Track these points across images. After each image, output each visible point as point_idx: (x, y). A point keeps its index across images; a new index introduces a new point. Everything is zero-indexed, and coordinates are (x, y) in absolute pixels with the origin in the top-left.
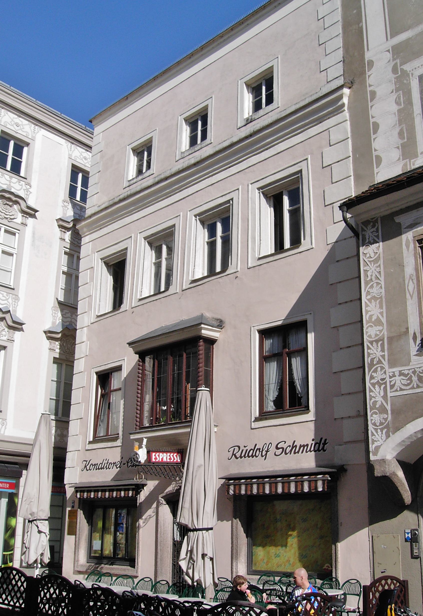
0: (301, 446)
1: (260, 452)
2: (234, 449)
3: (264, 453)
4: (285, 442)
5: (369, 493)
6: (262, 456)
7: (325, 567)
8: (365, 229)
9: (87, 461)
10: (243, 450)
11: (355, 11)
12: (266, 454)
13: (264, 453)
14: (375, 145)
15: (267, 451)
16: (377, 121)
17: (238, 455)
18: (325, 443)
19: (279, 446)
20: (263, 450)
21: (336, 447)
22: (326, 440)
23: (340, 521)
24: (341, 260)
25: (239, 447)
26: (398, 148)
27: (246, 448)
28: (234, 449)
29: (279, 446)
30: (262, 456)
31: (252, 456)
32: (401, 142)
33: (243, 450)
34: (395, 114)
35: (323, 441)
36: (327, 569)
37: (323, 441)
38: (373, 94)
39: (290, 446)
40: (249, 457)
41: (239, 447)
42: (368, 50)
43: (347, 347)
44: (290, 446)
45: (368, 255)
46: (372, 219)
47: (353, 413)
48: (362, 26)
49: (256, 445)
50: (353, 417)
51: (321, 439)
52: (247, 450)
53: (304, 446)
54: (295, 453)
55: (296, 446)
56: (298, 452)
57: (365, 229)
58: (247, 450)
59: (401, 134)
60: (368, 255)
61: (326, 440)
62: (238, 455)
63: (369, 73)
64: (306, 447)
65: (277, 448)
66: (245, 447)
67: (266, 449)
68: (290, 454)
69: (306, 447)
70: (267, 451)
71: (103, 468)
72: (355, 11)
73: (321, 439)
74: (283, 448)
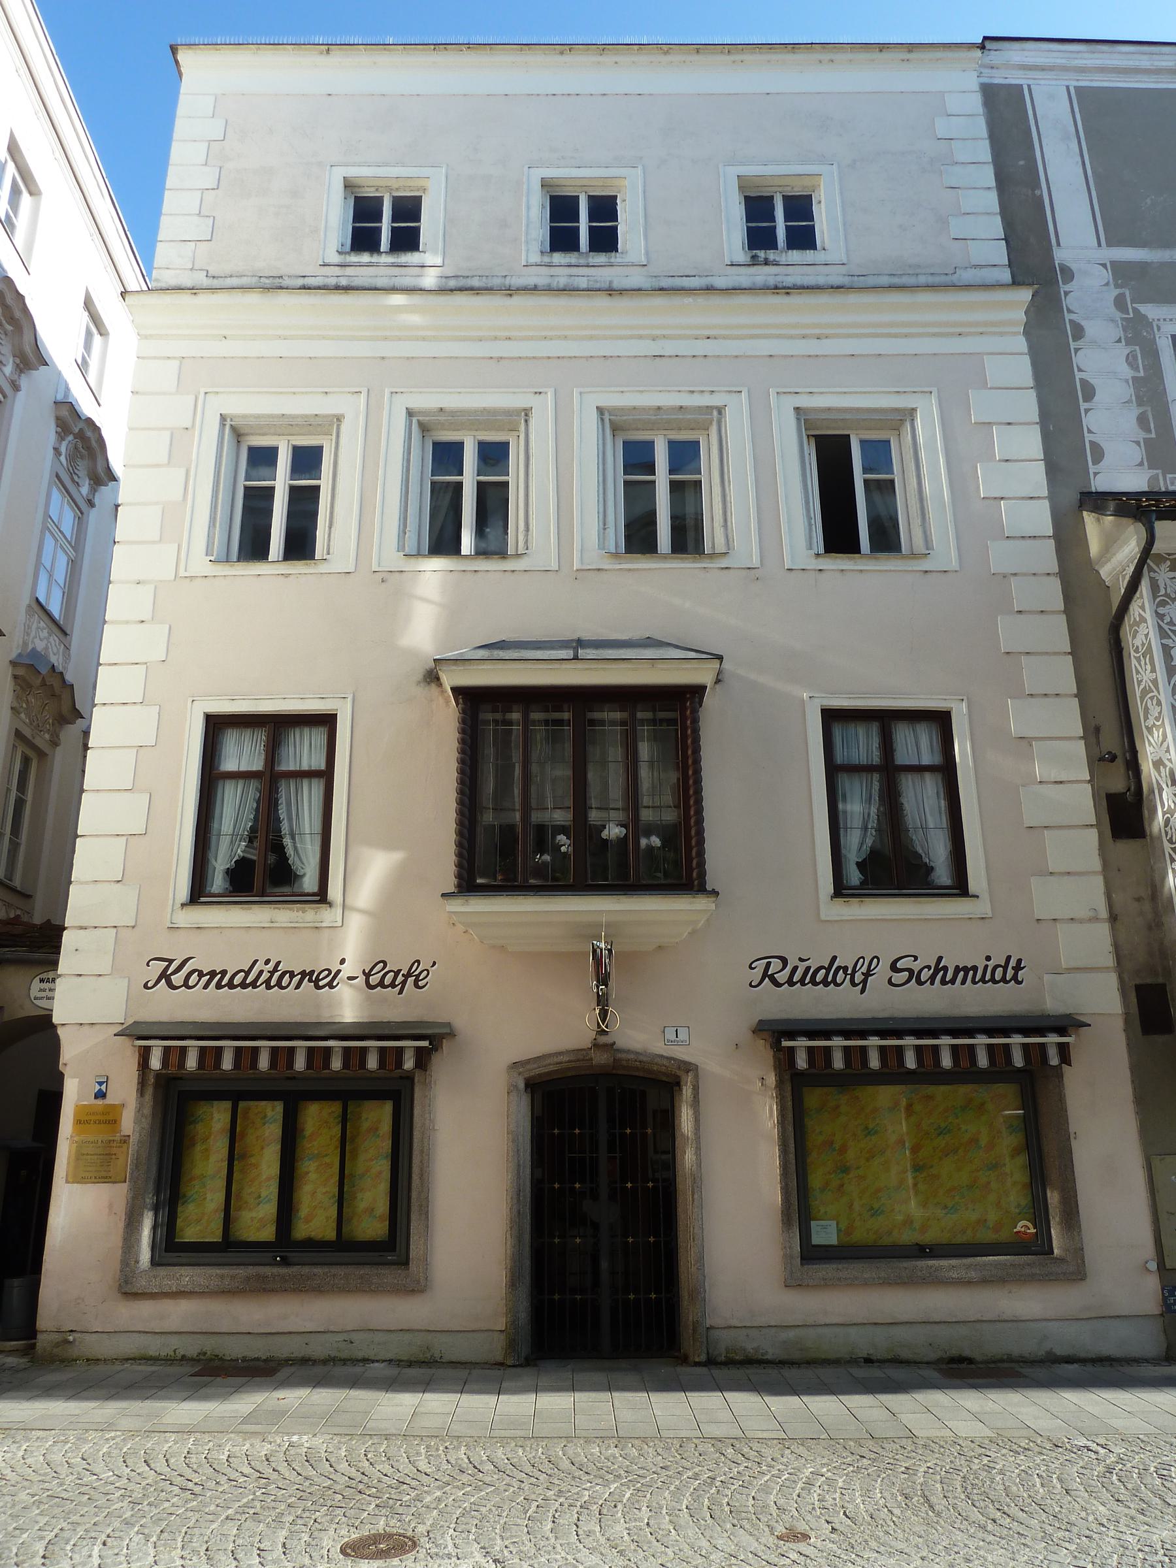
0: (957, 970)
1: (846, 974)
2: (769, 964)
3: (858, 977)
4: (916, 958)
5: (1132, 1072)
6: (854, 984)
7: (1018, 1229)
8: (1155, 567)
9: (171, 961)
10: (795, 969)
11: (1022, 163)
12: (865, 982)
13: (858, 977)
14: (1088, 421)
15: (867, 975)
16: (1092, 381)
17: (782, 977)
18: (1018, 967)
19: (899, 965)
20: (854, 971)
21: (1046, 977)
22: (1019, 961)
23: (1072, 1129)
24: (1029, 612)
25: (784, 961)
26: (1138, 443)
27: (807, 964)
28: (769, 964)
29: (899, 965)
30: (945, 969)
31: (825, 983)
32: (1141, 435)
33: (795, 969)
34: (1127, 381)
35: (1013, 963)
36: (1026, 1234)
37: (1013, 963)
38: (1079, 331)
39: (929, 967)
40: (815, 984)
41: (784, 961)
42: (1058, 244)
43: (1056, 782)
44: (929, 967)
45: (1167, 619)
46: (1169, 554)
47: (1084, 913)
48: (1041, 195)
49: (834, 958)
50: (1081, 921)
51: (1009, 958)
52: (808, 968)
53: (966, 970)
54: (943, 982)
55: (945, 969)
56: (953, 981)
57: (1155, 567)
58: (808, 968)
59: (1142, 421)
60: (1167, 619)
61: (1019, 961)
62: (782, 977)
63: (1067, 288)
64: (971, 973)
65: (894, 968)
66: (801, 960)
67: (864, 970)
68: (932, 983)
69: (971, 973)
70: (867, 975)
71: (254, 984)
72: (1022, 163)
73: (1009, 958)
74: (911, 971)
